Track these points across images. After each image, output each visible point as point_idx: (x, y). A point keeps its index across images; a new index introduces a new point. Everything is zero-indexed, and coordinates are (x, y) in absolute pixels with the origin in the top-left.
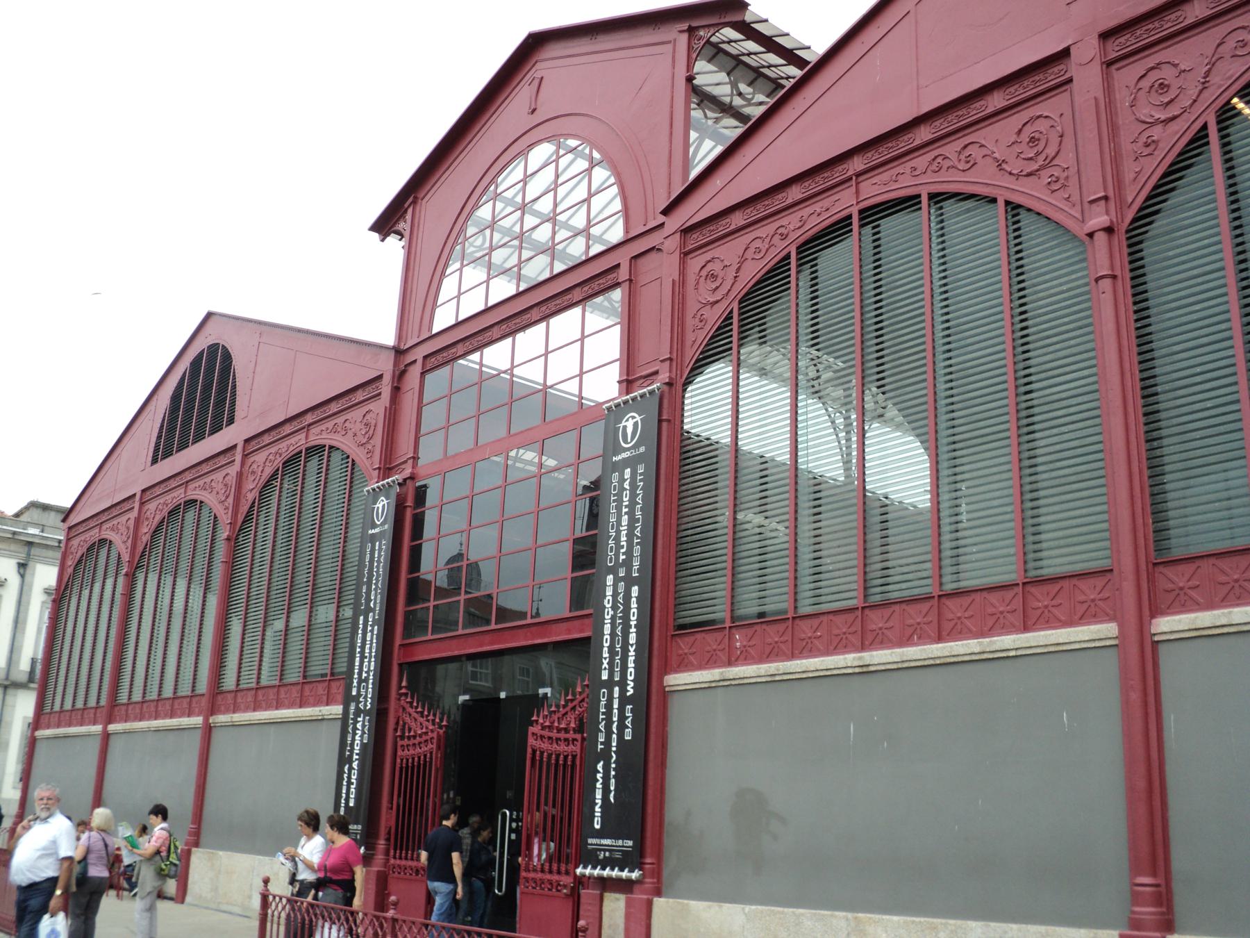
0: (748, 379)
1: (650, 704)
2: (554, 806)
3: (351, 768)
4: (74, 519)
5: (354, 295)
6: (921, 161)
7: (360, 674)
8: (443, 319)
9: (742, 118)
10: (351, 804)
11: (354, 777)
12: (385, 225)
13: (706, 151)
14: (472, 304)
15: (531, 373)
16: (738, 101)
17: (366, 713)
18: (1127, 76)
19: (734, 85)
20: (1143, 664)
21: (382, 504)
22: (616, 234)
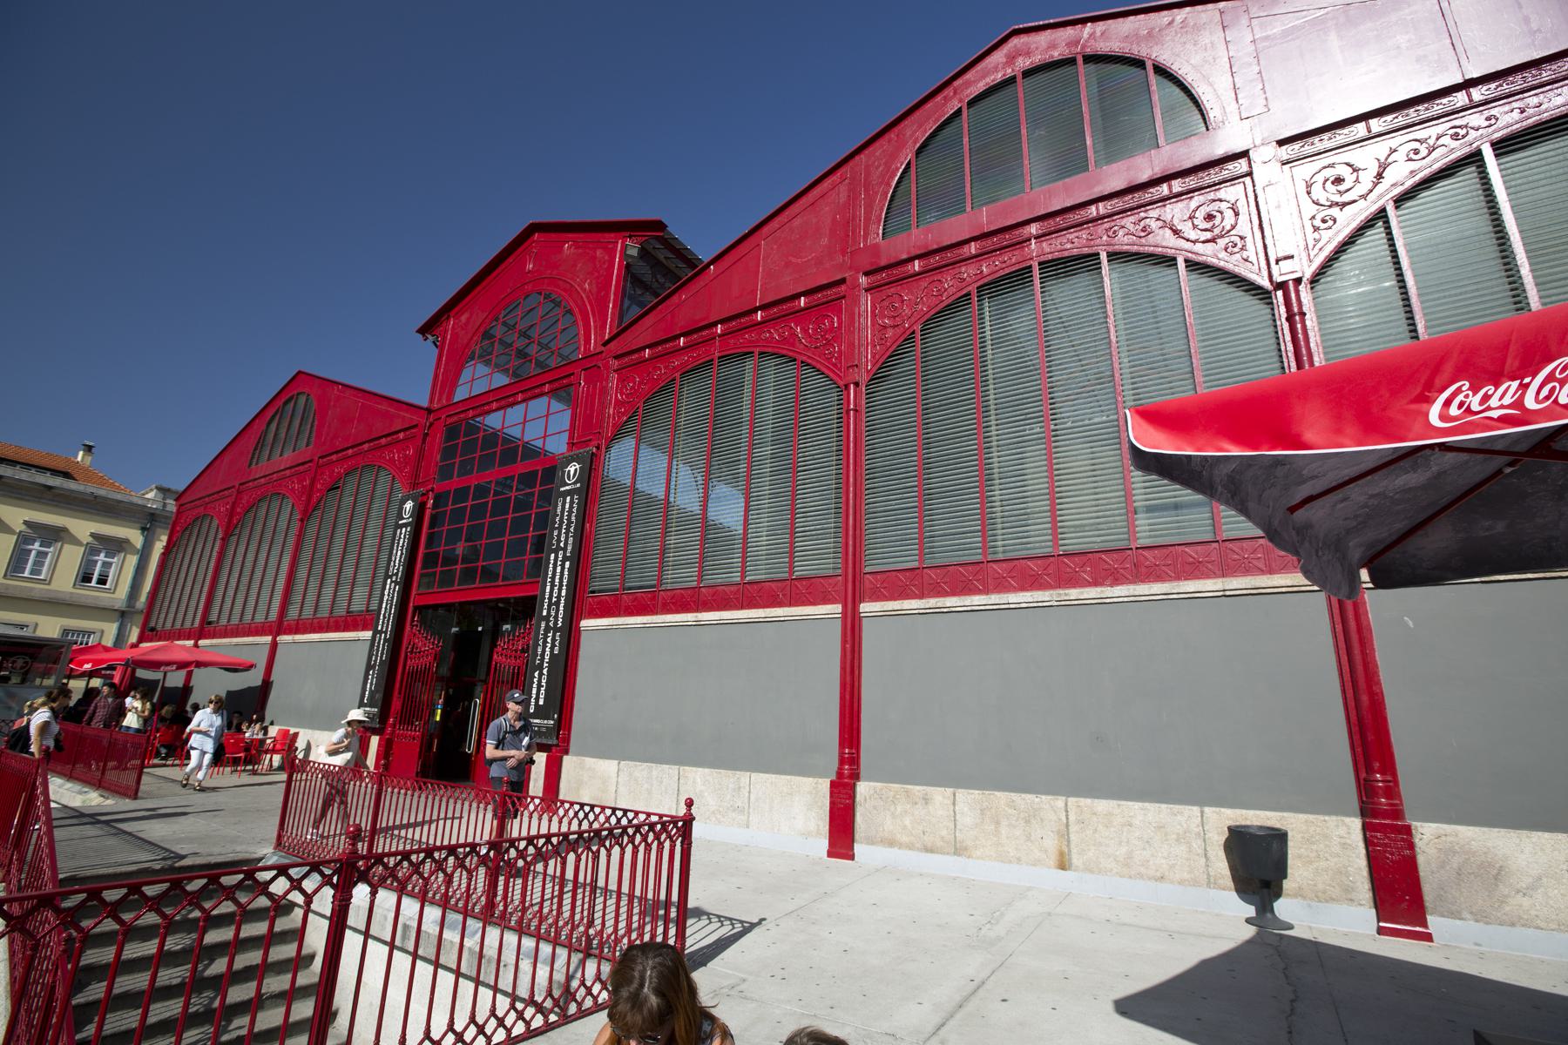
0: (645, 451)
1: (571, 637)
3: (541, 674)
4: (183, 501)
7: (550, 598)
8: (461, 394)
10: (541, 702)
11: (544, 682)
12: (424, 330)
14: (480, 388)
15: (515, 432)
16: (655, 285)
17: (556, 630)
19: (654, 275)
20: (852, 629)
21: (409, 505)
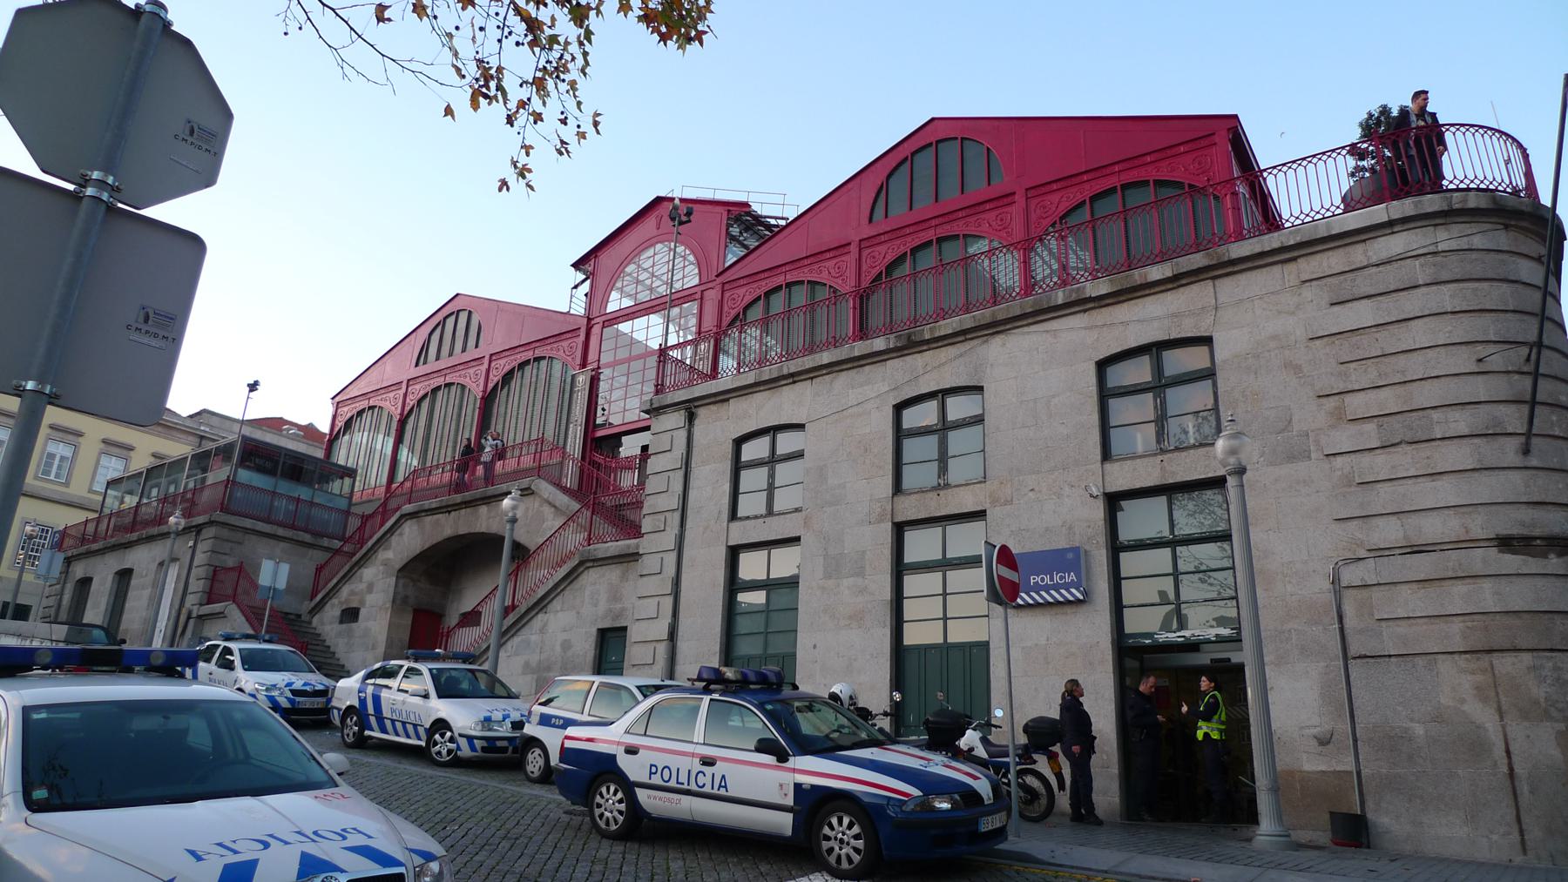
2: (51, 456)
5: (561, 293)
6: (961, 223)
9: (746, 247)
13: (731, 259)
18: (1034, 202)
22: (696, 281)
